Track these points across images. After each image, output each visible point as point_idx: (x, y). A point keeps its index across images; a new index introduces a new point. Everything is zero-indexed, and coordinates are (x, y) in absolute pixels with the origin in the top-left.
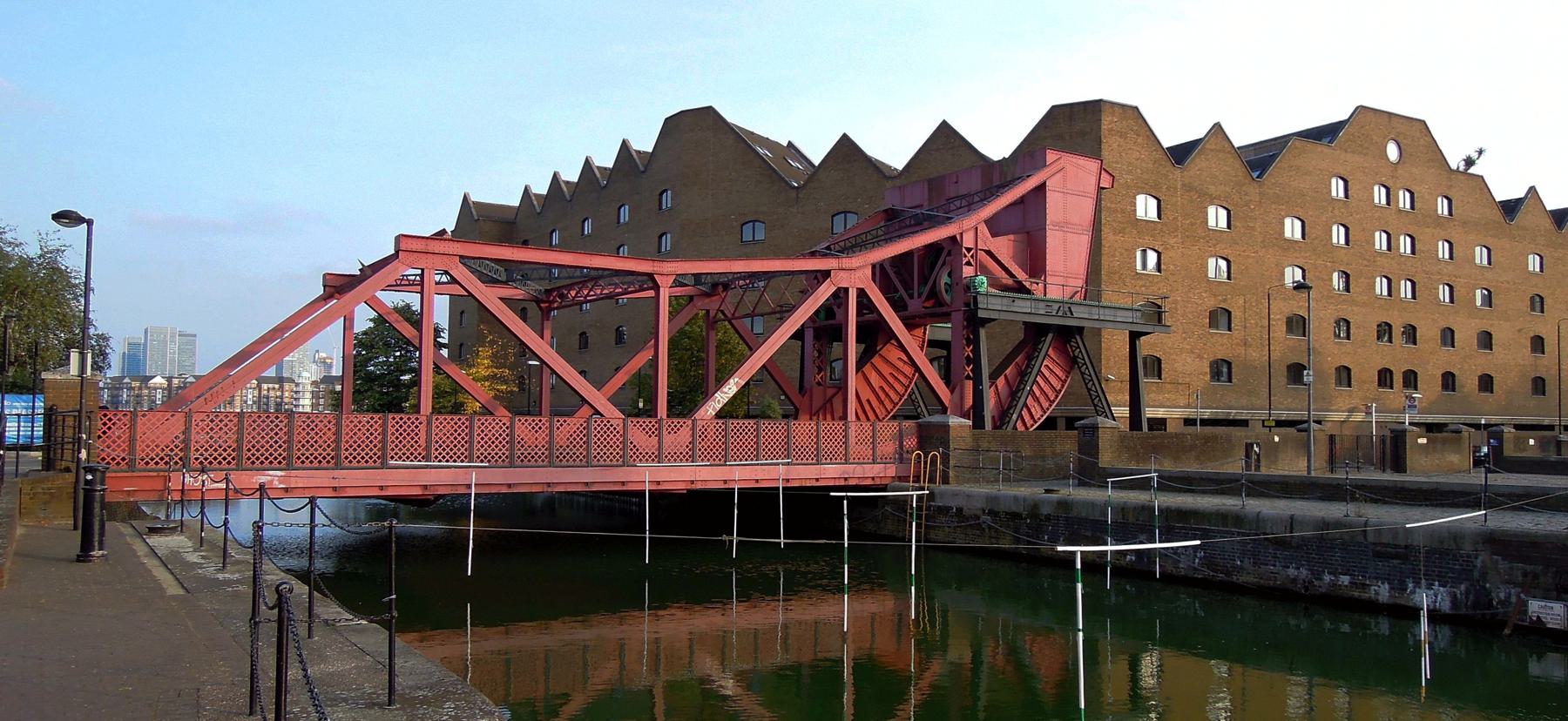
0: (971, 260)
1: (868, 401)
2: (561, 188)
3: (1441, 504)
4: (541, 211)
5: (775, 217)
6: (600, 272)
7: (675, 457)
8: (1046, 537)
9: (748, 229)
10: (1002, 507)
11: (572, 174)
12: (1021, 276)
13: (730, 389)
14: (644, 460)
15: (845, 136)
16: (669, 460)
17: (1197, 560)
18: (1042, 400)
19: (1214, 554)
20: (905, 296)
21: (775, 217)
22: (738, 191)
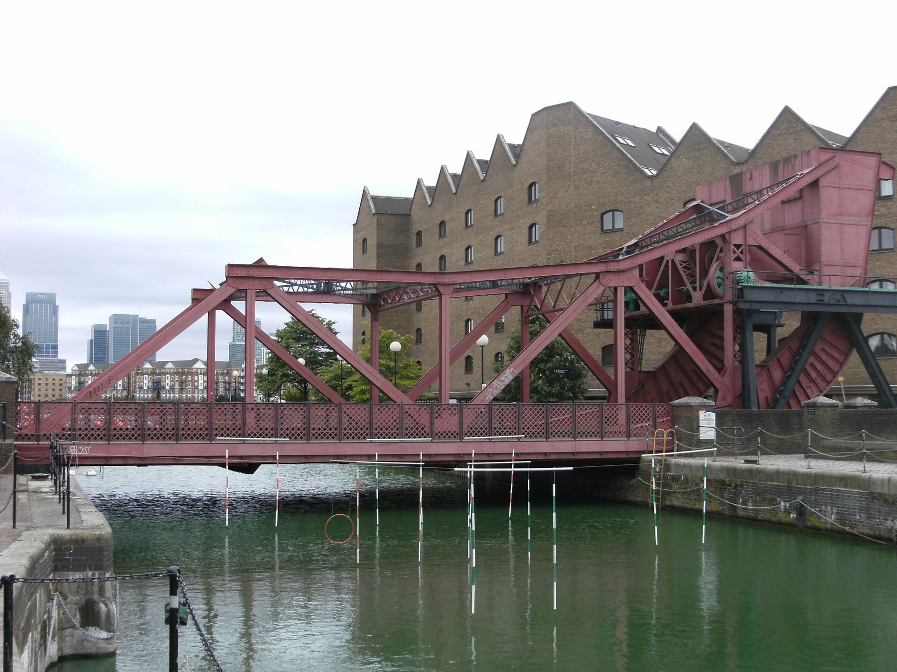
0: (741, 256)
1: (681, 383)
2: (504, 150)
4: (517, 163)
5: (632, 206)
6: (397, 284)
7: (587, 434)
8: (741, 501)
9: (608, 217)
11: (456, 167)
12: (796, 268)
13: (506, 377)
14: (556, 436)
15: (787, 111)
16: (439, 437)
17: (833, 516)
18: (818, 381)
19: (843, 511)
20: (691, 290)
21: (632, 206)
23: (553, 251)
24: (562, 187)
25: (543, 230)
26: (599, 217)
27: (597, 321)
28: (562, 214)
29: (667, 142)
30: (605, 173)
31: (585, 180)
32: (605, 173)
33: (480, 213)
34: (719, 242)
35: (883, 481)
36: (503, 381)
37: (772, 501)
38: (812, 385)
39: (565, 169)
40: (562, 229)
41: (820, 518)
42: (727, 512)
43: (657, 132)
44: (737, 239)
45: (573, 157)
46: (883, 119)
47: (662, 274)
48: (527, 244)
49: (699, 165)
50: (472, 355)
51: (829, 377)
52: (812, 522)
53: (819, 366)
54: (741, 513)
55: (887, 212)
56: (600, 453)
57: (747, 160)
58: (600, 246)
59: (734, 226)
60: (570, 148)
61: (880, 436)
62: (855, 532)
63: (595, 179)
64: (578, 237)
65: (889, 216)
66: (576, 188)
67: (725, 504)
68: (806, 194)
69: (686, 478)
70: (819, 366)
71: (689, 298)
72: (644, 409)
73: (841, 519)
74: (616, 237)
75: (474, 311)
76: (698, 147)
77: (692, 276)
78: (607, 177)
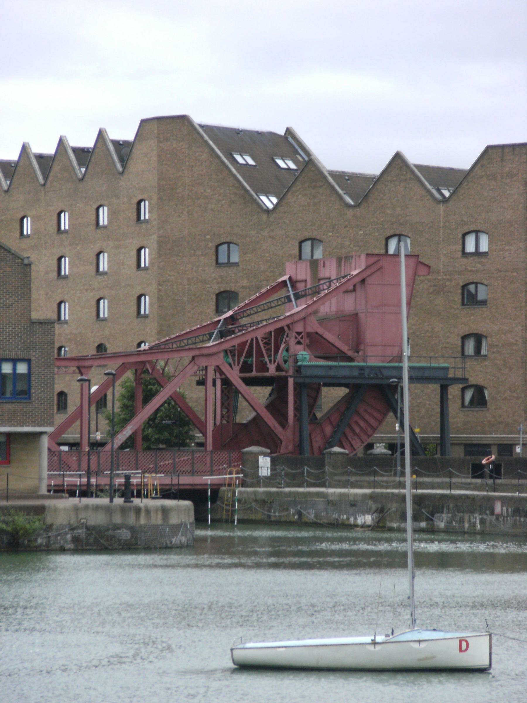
0: (301, 341)
3: (319, 563)
5: (248, 240)
7: (184, 473)
10: (259, 497)
12: (345, 348)
20: (268, 362)
22: (212, 210)
23: (164, 282)
24: (175, 211)
25: (153, 256)
26: (214, 249)
27: (200, 380)
28: (174, 241)
29: (297, 147)
30: (220, 201)
31: (200, 206)
32: (220, 201)
33: (77, 219)
34: (286, 328)
35: (332, 493)
36: (125, 435)
37: (287, 510)
38: (356, 438)
39: (178, 191)
40: (175, 258)
41: (307, 517)
42: (266, 519)
43: (285, 134)
44: (299, 328)
45: (187, 178)
46: (482, 177)
47: (249, 346)
48: (135, 269)
49: (315, 204)
50: (66, 390)
51: (370, 431)
52: (305, 519)
53: (362, 423)
54: (273, 519)
55: (482, 268)
56: (192, 485)
57: (359, 204)
58: (215, 281)
59: (296, 318)
60: (183, 168)
61: (385, 471)
62: (322, 522)
63: (210, 206)
64: (192, 269)
65: (484, 272)
66: (190, 213)
67: (264, 514)
68: (358, 288)
69: (245, 500)
70: (362, 423)
71: (267, 370)
72: (224, 455)
73: (316, 516)
74: (231, 272)
75: (69, 337)
76: (314, 184)
77: (269, 350)
78: (222, 205)
